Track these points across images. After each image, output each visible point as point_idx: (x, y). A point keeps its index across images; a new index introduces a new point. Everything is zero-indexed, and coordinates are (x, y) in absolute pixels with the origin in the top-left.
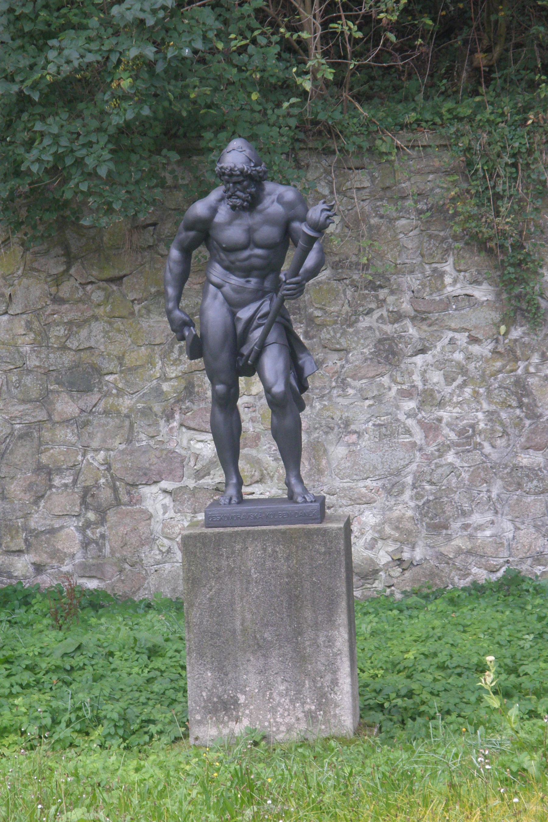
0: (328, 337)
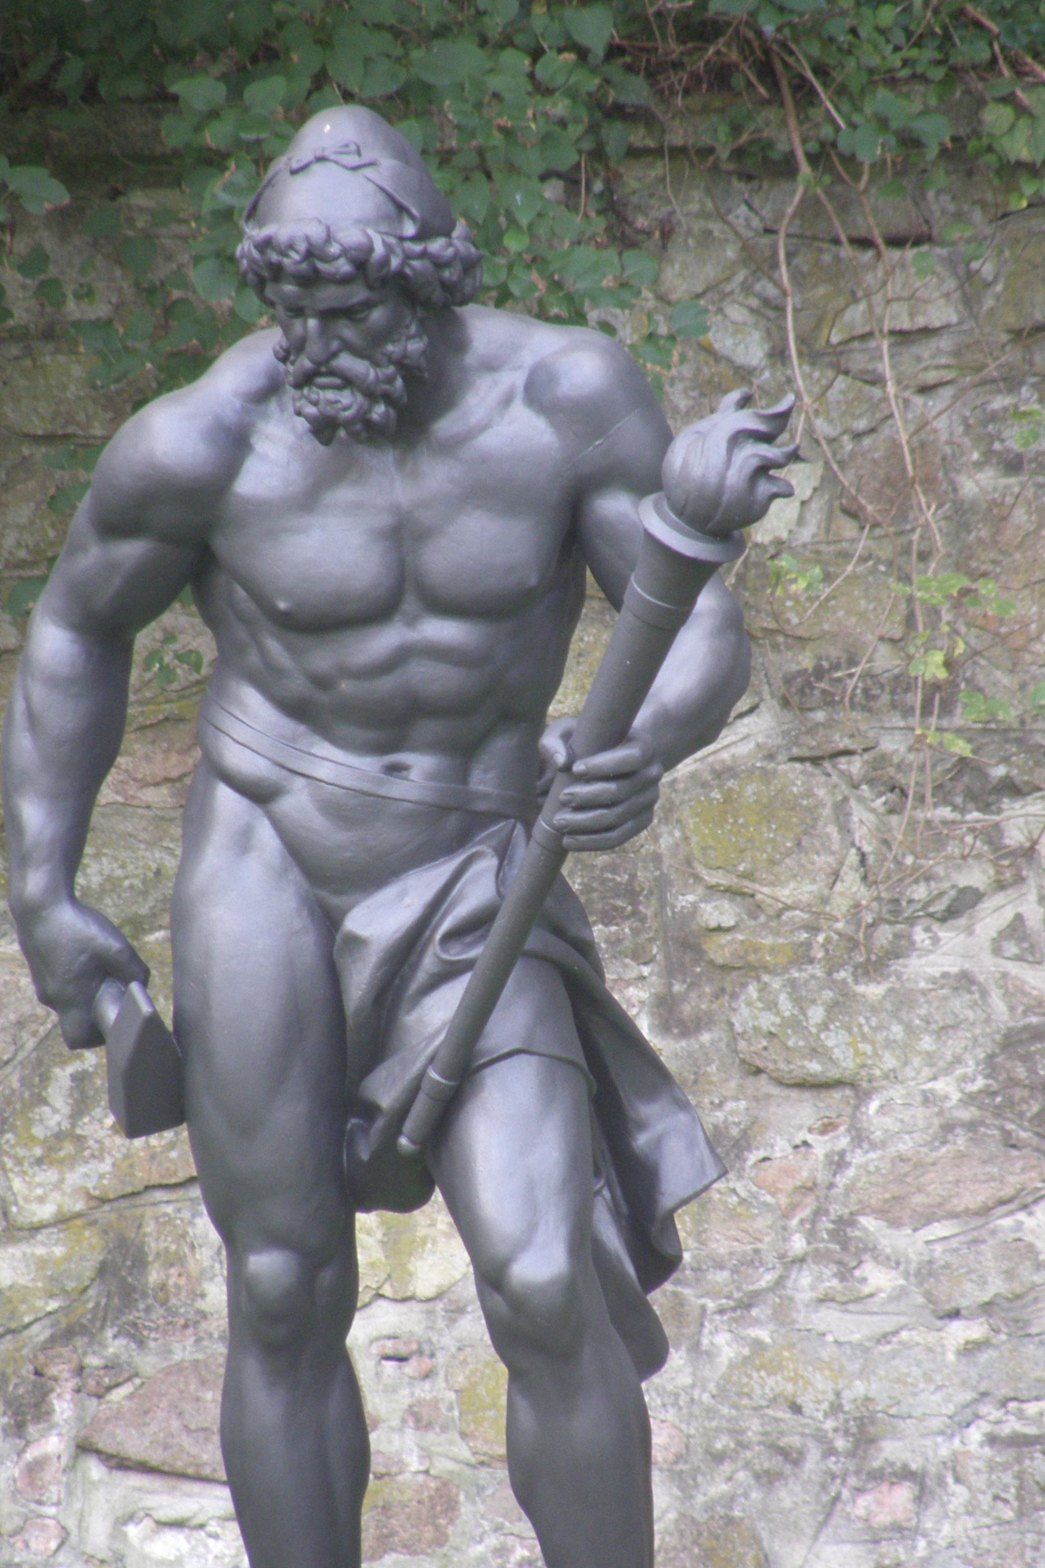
0: (768, 1021)
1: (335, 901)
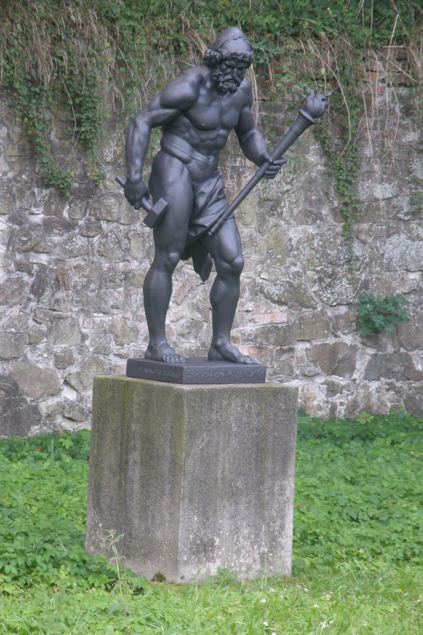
1: (196, 185)
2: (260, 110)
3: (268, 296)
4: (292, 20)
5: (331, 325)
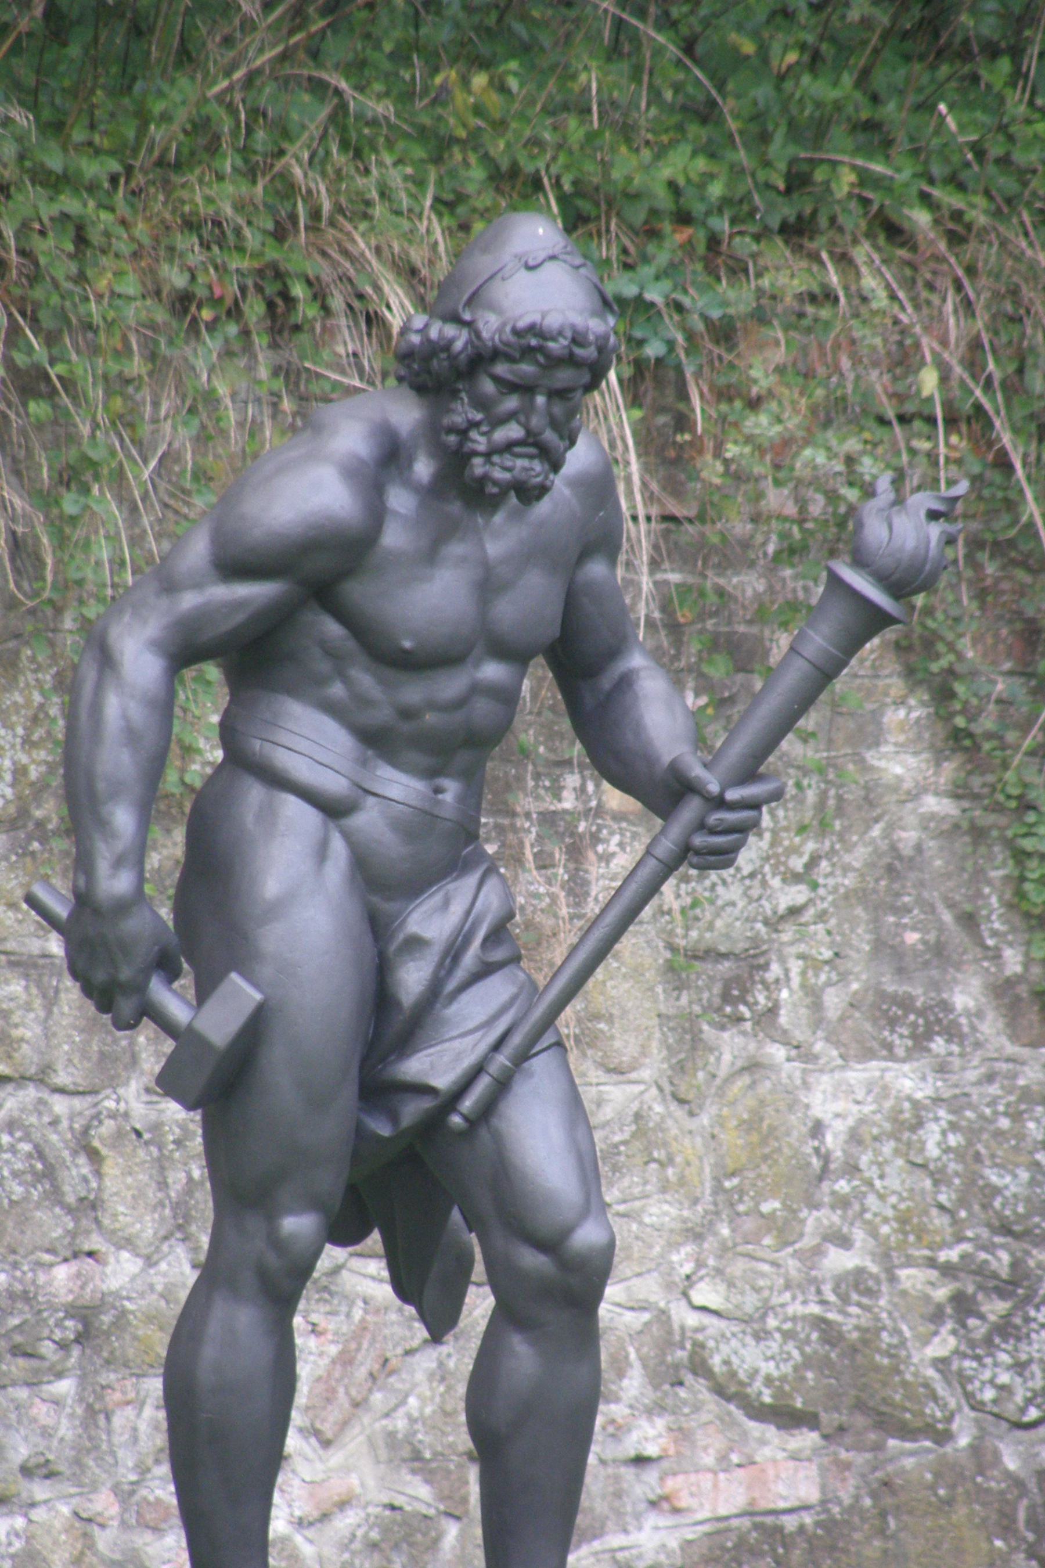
1: (388, 907)
2: (655, 565)
3: (730, 1390)
4: (782, 166)
5: (1022, 1516)
